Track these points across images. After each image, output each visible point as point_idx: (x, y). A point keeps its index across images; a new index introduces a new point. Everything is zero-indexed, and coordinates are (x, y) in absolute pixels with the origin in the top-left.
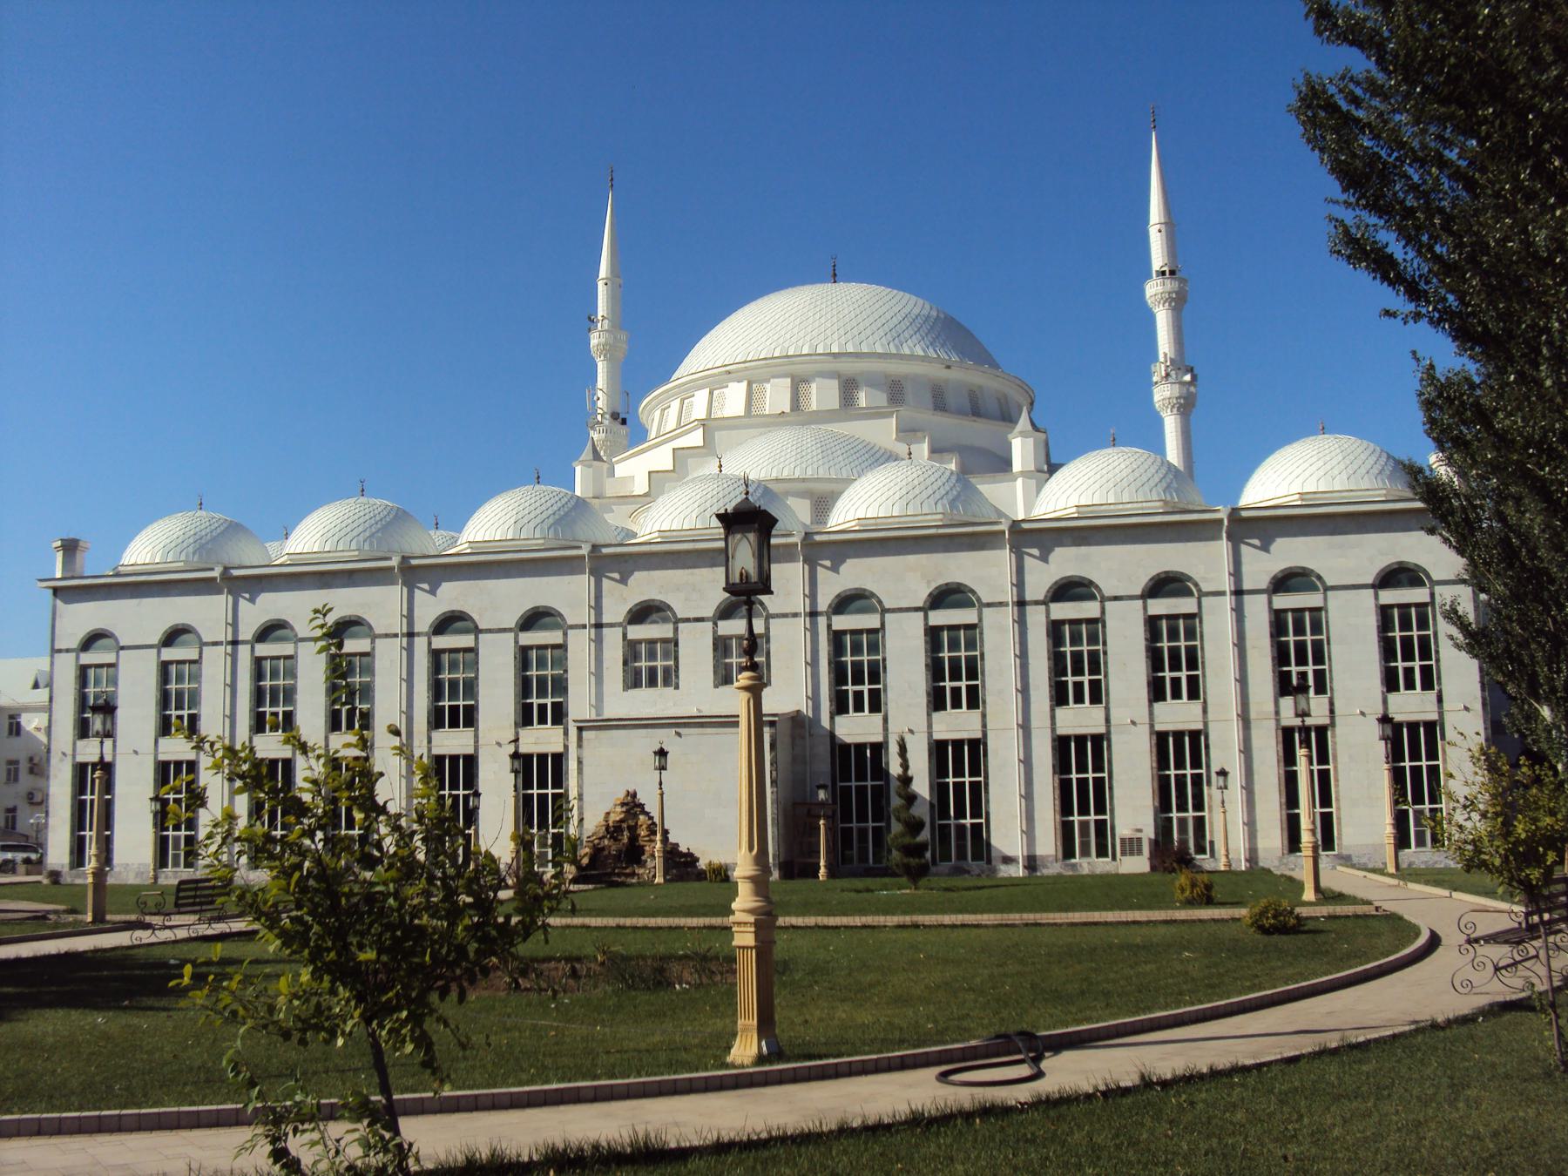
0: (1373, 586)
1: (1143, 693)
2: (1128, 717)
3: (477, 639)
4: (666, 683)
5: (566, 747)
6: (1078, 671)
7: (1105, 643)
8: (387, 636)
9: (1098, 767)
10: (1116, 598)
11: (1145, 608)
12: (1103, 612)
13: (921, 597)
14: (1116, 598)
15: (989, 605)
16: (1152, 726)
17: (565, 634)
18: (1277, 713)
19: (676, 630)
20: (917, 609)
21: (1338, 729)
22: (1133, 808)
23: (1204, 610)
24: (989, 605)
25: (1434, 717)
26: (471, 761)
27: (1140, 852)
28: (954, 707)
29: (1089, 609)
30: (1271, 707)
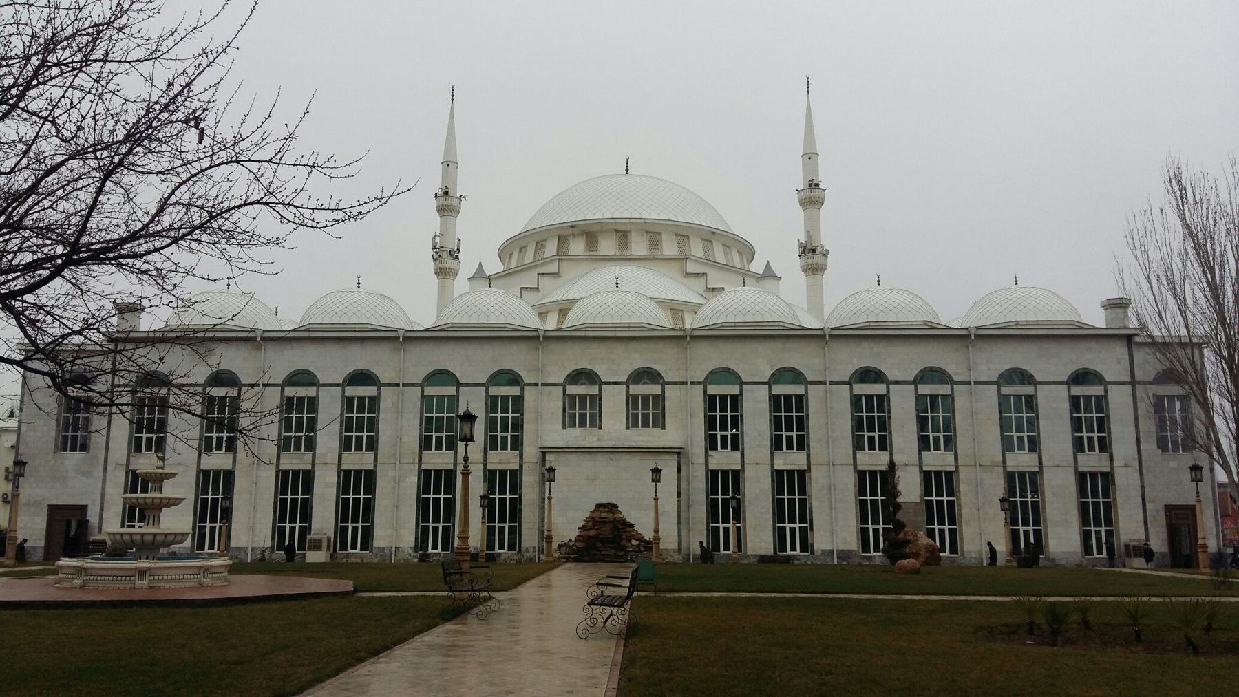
0: (1067, 383)
1: (915, 445)
2: (757, 462)
3: (458, 390)
4: (655, 425)
5: (455, 464)
6: (1020, 430)
7: (889, 412)
8: (390, 385)
9: (950, 494)
10: (897, 383)
11: (916, 390)
12: (888, 391)
13: (766, 375)
14: (897, 383)
15: (812, 383)
16: (921, 467)
17: (522, 390)
18: (1004, 462)
19: (600, 390)
20: (338, 385)
21: (1045, 475)
22: (323, 518)
23: (956, 394)
24: (812, 383)
25: (1107, 470)
26: (371, 475)
27: (320, 549)
28: (1019, 450)
29: (879, 389)
30: (1000, 459)
